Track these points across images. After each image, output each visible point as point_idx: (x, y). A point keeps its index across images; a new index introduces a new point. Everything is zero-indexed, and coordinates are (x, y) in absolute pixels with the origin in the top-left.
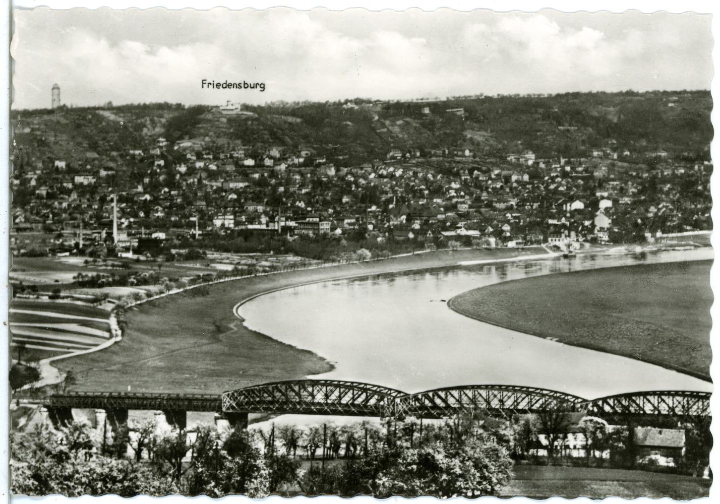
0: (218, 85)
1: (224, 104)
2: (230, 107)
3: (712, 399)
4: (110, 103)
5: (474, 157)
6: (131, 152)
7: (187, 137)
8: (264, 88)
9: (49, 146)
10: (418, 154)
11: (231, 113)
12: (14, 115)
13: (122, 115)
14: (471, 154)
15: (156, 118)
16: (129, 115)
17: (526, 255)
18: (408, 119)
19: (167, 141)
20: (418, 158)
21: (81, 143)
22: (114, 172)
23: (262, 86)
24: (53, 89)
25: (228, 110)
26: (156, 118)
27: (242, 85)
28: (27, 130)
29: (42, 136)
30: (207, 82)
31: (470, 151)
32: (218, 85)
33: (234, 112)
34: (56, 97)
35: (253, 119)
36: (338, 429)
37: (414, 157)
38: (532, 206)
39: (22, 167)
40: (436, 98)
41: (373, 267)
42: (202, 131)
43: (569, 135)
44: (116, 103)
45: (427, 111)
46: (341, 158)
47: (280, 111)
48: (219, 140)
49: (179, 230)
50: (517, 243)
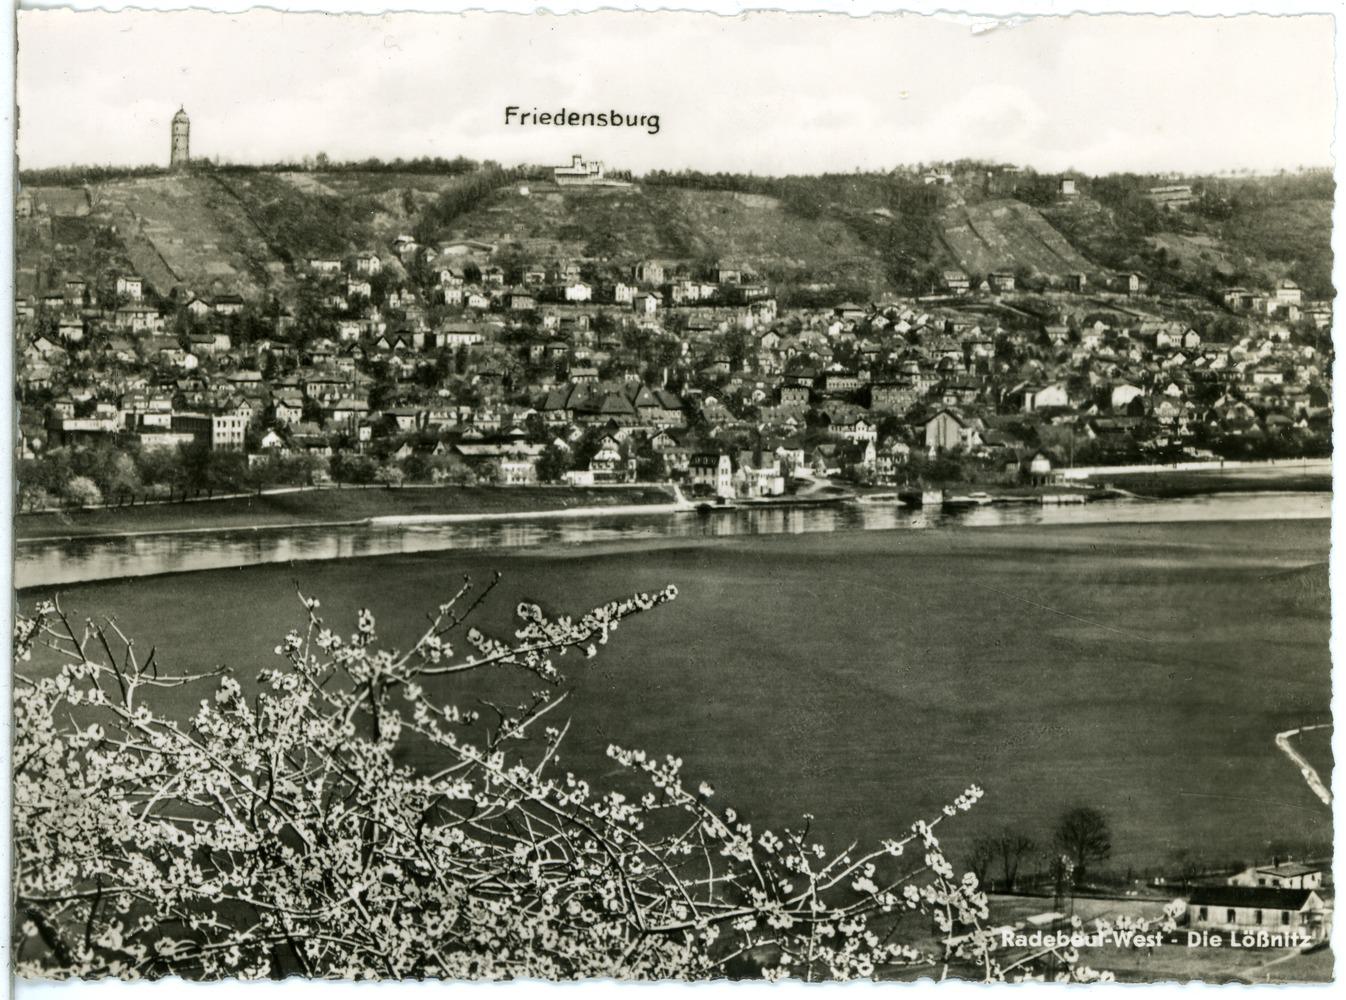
0: (544, 119)
2: (579, 170)
3: (1332, 945)
4: (322, 157)
5: (1149, 293)
6: (315, 264)
8: (657, 125)
11: (579, 181)
12: (26, 180)
14: (1144, 286)
16: (356, 183)
17: (608, 504)
19: (417, 241)
21: (201, 242)
23: (653, 121)
27: (608, 118)
29: (111, 223)
30: (519, 112)
31: (1141, 279)
32: (544, 119)
33: (588, 181)
34: (181, 144)
35: (624, 198)
36: (352, 972)
39: (394, 317)
40: (1301, 169)
41: (163, 520)
42: (501, 221)
44: (337, 157)
46: (815, 287)
47: (526, 173)
48: (533, 241)
50: (598, 477)
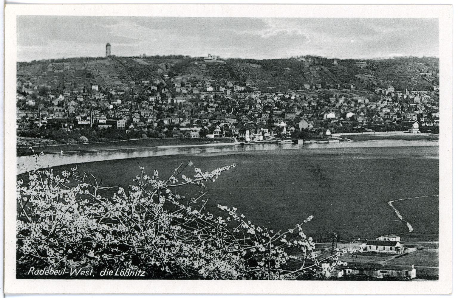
1: (207, 56)
2: (210, 58)
7: (180, 74)
9: (93, 77)
10: (320, 87)
11: (210, 61)
13: (148, 61)
14: (355, 87)
15: (168, 64)
18: (323, 67)
20: (320, 89)
22: (123, 93)
24: (107, 46)
25: (208, 59)
26: (168, 64)
28: (83, 68)
29: (91, 71)
31: (354, 86)
33: (212, 61)
34: (108, 52)
37: (317, 88)
38: (307, 116)
43: (425, 78)
45: (335, 62)
49: (376, 133)
50: (215, 136)
